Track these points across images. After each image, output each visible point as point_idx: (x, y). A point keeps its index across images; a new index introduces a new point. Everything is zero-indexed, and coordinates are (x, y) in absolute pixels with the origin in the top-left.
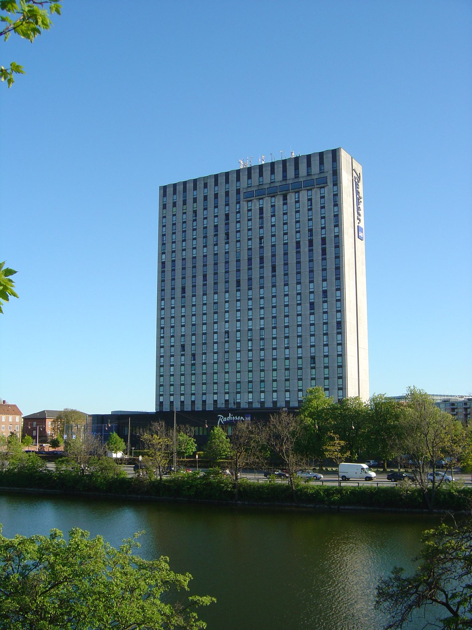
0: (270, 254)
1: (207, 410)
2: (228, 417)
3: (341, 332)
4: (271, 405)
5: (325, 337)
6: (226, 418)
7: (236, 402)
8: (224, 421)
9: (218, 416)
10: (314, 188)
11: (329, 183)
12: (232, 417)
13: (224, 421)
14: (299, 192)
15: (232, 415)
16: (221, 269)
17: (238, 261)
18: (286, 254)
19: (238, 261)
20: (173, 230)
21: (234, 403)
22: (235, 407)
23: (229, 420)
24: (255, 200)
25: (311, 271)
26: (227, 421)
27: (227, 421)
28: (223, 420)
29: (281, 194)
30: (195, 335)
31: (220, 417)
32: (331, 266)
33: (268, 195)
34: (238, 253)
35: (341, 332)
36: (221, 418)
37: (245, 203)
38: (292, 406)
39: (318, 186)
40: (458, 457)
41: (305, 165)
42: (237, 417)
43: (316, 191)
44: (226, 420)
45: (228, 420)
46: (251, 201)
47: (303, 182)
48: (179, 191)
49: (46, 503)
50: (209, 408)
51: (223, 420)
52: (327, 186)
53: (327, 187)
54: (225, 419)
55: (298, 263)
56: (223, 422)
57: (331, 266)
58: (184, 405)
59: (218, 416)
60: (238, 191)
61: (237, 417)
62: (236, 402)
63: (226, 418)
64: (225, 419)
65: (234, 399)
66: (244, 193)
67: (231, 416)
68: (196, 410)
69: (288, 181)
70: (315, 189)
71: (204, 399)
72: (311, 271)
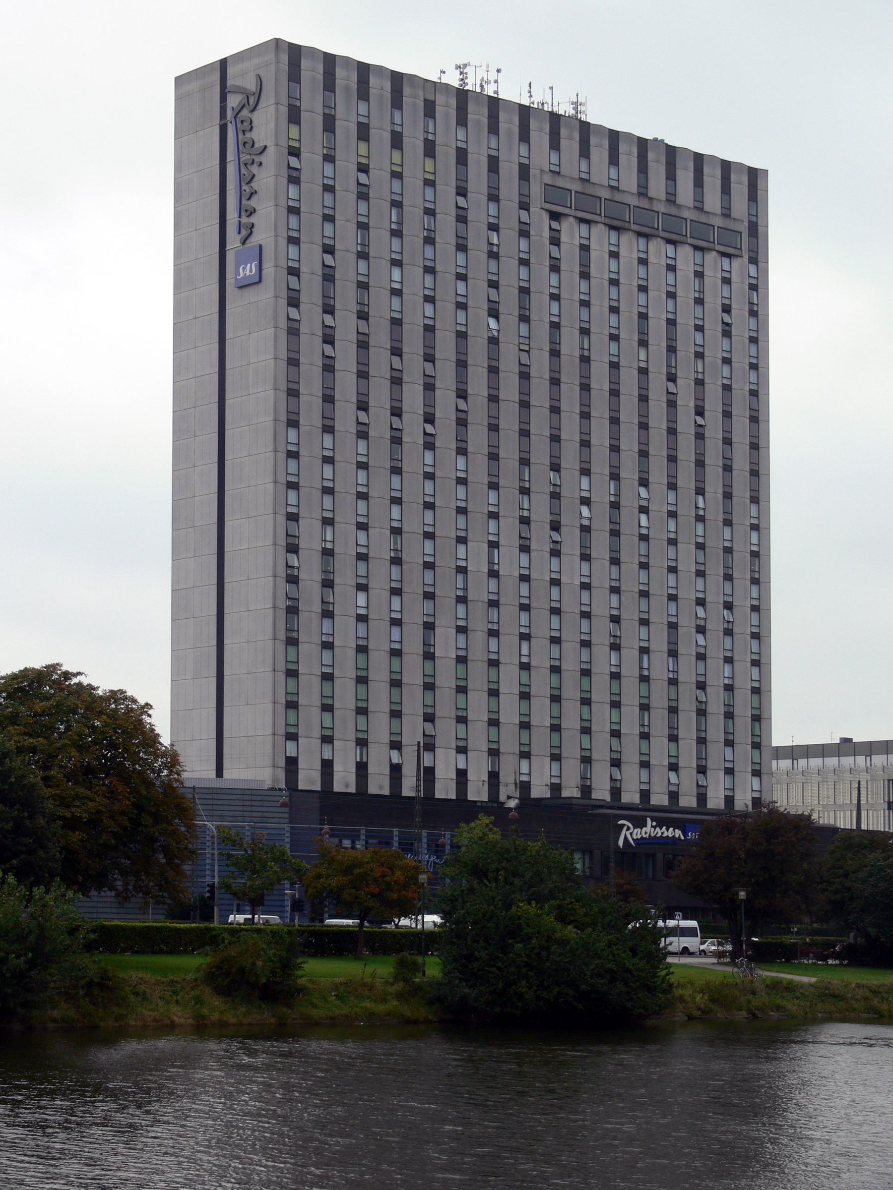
2: (644, 829)
4: (636, 799)
6: (639, 830)
7: (518, 782)
9: (620, 822)
10: (714, 250)
16: (600, 436)
21: (516, 783)
23: (647, 836)
26: (642, 837)
27: (642, 837)
28: (631, 834)
29: (546, 210)
31: (625, 825)
32: (741, 464)
42: (667, 830)
44: (639, 837)
45: (644, 836)
49: (813, 1156)
51: (631, 834)
52: (742, 257)
53: (740, 259)
54: (638, 833)
56: (632, 842)
57: (741, 464)
59: (620, 822)
61: (667, 830)
62: (518, 782)
67: (652, 826)
68: (403, 795)
70: (714, 253)
71: (327, 756)
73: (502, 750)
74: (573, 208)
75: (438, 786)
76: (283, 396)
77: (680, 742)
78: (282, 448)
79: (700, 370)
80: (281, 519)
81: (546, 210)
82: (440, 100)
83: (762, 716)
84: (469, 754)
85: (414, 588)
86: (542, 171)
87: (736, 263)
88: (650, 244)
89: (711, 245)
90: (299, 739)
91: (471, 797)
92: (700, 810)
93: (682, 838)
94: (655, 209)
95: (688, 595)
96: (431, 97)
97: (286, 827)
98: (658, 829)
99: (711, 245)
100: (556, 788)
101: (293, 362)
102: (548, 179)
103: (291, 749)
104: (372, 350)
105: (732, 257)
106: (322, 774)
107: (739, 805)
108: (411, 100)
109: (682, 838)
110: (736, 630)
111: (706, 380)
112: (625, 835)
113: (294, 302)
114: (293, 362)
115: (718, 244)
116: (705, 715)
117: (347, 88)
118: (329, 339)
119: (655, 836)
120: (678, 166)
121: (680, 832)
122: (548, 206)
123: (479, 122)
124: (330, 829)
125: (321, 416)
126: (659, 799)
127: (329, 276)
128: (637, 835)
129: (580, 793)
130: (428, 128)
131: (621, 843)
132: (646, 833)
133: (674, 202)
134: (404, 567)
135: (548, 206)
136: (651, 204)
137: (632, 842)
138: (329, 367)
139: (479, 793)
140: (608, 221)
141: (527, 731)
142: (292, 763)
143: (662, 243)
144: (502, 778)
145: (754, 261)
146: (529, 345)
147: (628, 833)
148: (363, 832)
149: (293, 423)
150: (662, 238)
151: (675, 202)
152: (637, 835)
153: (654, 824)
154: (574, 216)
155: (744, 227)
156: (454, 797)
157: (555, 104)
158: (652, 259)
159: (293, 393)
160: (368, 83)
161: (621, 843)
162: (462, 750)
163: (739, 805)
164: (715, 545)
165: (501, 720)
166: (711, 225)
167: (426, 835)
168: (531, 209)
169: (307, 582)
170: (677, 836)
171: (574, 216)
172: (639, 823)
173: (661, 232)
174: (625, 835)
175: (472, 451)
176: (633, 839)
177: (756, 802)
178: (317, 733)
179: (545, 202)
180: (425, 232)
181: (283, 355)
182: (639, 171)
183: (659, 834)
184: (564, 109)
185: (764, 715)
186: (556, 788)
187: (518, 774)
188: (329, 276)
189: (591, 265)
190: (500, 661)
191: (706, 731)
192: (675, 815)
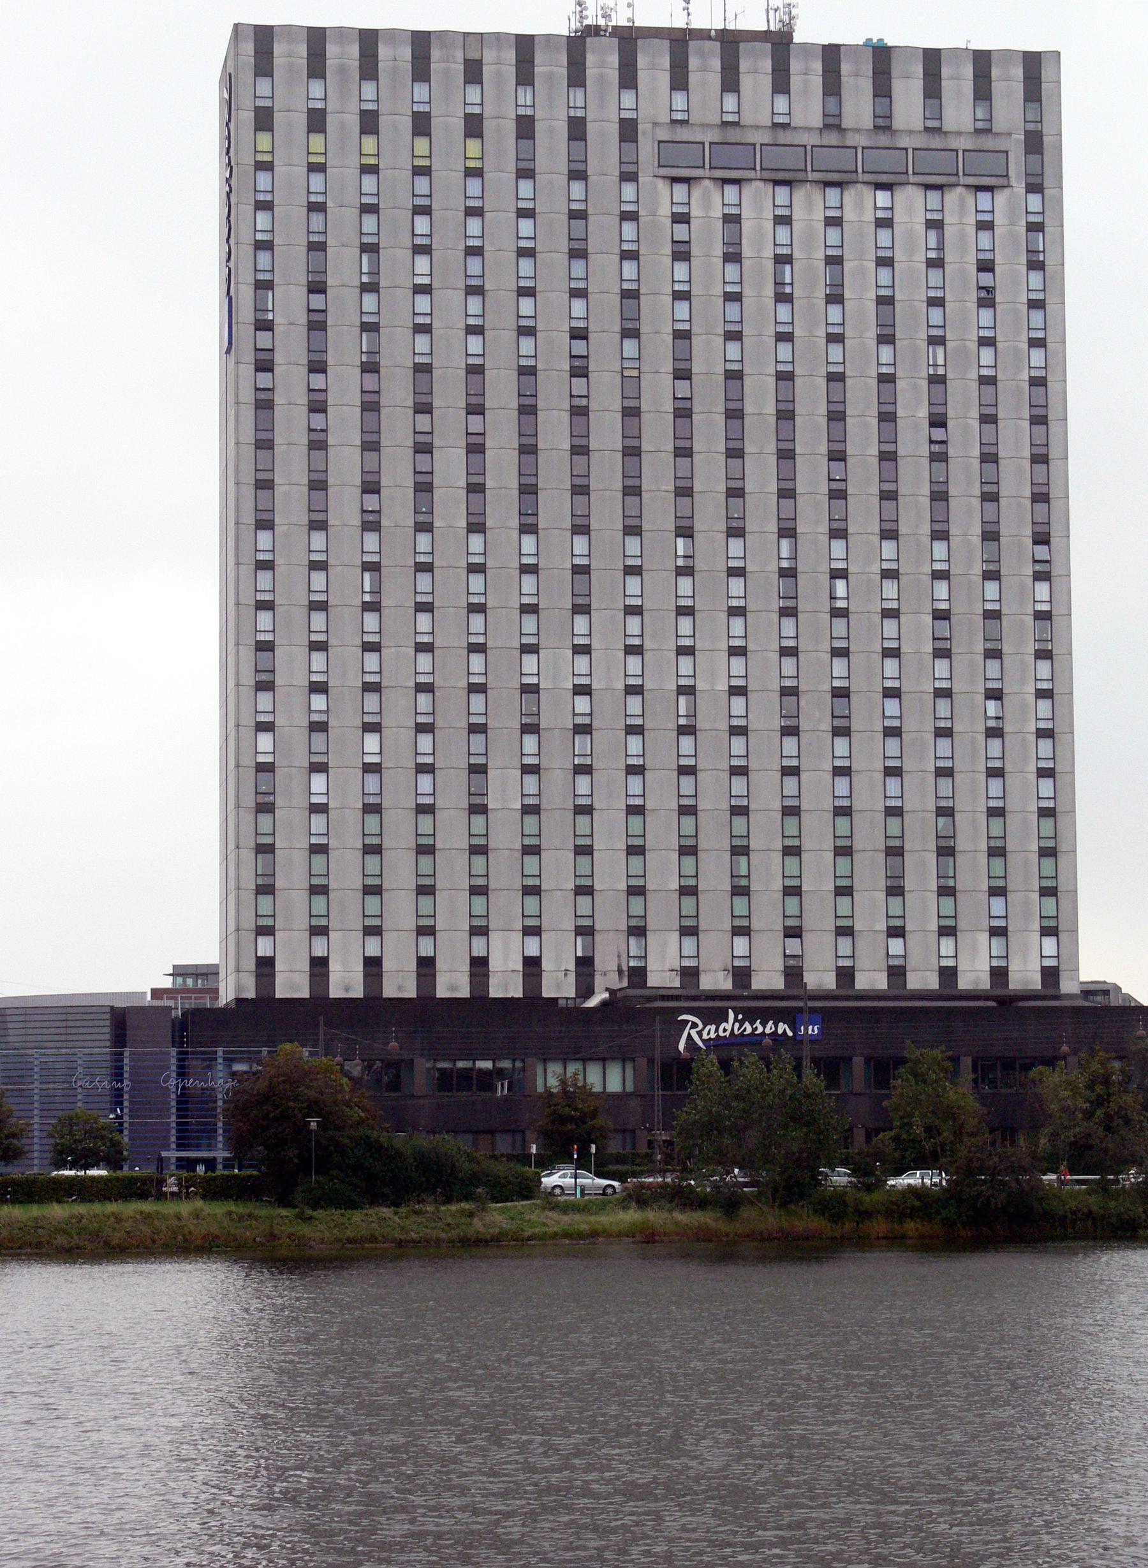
0: (771, 408)
1: (493, 994)
3: (1053, 730)
4: (777, 983)
6: (713, 1027)
7: (625, 968)
8: (705, 1037)
10: (958, 185)
11: (1013, 182)
12: (742, 1023)
13: (705, 1037)
15: (740, 1017)
17: (631, 413)
18: (837, 416)
19: (631, 413)
20: (518, 238)
22: (625, 983)
23: (728, 1033)
24: (707, 182)
25: (940, 496)
29: (664, 177)
31: (689, 1021)
33: (766, 175)
34: (631, 384)
35: (1053, 730)
36: (694, 1025)
37: (662, 187)
38: (918, 987)
40: (979, 1195)
41: (916, 85)
42: (764, 1025)
43: (962, 202)
44: (713, 1035)
45: (721, 1034)
47: (860, 150)
48: (395, 71)
51: (700, 1033)
52: (1009, 186)
53: (1007, 191)
54: (710, 1032)
55: (888, 457)
56: (700, 1044)
60: (628, 131)
61: (764, 1025)
62: (625, 968)
63: (713, 1027)
64: (710, 1032)
65: (619, 956)
66: (660, 142)
67: (736, 1020)
69: (849, 135)
70: (959, 190)
71: (319, 952)
72: (940, 496)
73: (597, 927)
74: (707, 166)
75: (493, 981)
76: (249, 491)
77: (907, 895)
78: (248, 559)
79: (941, 361)
80: (247, 653)
81: (664, 177)
82: (489, 56)
83: (1058, 849)
84: (544, 935)
85: (453, 720)
86: (655, 124)
87: (1001, 197)
88: (846, 194)
89: (952, 179)
90: (276, 933)
91: (547, 993)
92: (843, 992)
93: (790, 1034)
94: (849, 144)
95: (919, 686)
96: (473, 55)
97: (173, 1051)
98: (747, 1025)
99: (952, 179)
101: (264, 444)
102: (663, 135)
103: (264, 947)
104: (384, 411)
105: (995, 190)
106: (310, 976)
107: (1016, 982)
108: (596, 71)
109: (790, 1034)
110: (1007, 729)
111: (949, 376)
112: (689, 1034)
113: (264, 365)
114: (264, 444)
115: (964, 174)
116: (954, 855)
117: (499, 77)
118: (318, 406)
119: (742, 1035)
120: (894, 73)
121: (786, 1026)
122: (664, 172)
123: (447, 72)
124: (224, 1051)
125: (306, 509)
126: (716, 980)
127: (317, 324)
128: (709, 1034)
129: (678, 979)
131: (682, 1046)
132: (725, 1030)
133: (838, 128)
134: (437, 694)
135: (664, 172)
136: (844, 137)
137: (700, 1044)
138: (318, 444)
139: (558, 986)
140: (766, 175)
141: (899, 899)
142: (265, 966)
143: (867, 192)
144: (598, 964)
145: (1035, 187)
146: (639, 368)
147: (693, 1033)
148: (220, 1054)
149: (265, 524)
151: (940, 129)
152: (709, 1034)
154: (710, 178)
155: (1015, 145)
156: (519, 994)
157: (730, 15)
158: (849, 215)
159: (264, 485)
160: (375, 56)
161: (682, 1046)
162: (689, 931)
163: (1016, 982)
164: (968, 613)
165: (596, 887)
166: (802, 146)
167: (307, 1054)
169: (287, 729)
170: (780, 1031)
171: (710, 178)
172: (715, 1016)
173: (707, 171)
174: (689, 1034)
175: (545, 527)
176: (703, 1041)
177: (1051, 975)
178: (303, 923)
179: (659, 166)
181: (249, 436)
182: (927, 96)
183: (749, 1030)
185: (1063, 846)
186: (999, 974)
187: (624, 956)
188: (317, 324)
189: (743, 242)
190: (594, 806)
191: (954, 877)
192: (1032, 1003)
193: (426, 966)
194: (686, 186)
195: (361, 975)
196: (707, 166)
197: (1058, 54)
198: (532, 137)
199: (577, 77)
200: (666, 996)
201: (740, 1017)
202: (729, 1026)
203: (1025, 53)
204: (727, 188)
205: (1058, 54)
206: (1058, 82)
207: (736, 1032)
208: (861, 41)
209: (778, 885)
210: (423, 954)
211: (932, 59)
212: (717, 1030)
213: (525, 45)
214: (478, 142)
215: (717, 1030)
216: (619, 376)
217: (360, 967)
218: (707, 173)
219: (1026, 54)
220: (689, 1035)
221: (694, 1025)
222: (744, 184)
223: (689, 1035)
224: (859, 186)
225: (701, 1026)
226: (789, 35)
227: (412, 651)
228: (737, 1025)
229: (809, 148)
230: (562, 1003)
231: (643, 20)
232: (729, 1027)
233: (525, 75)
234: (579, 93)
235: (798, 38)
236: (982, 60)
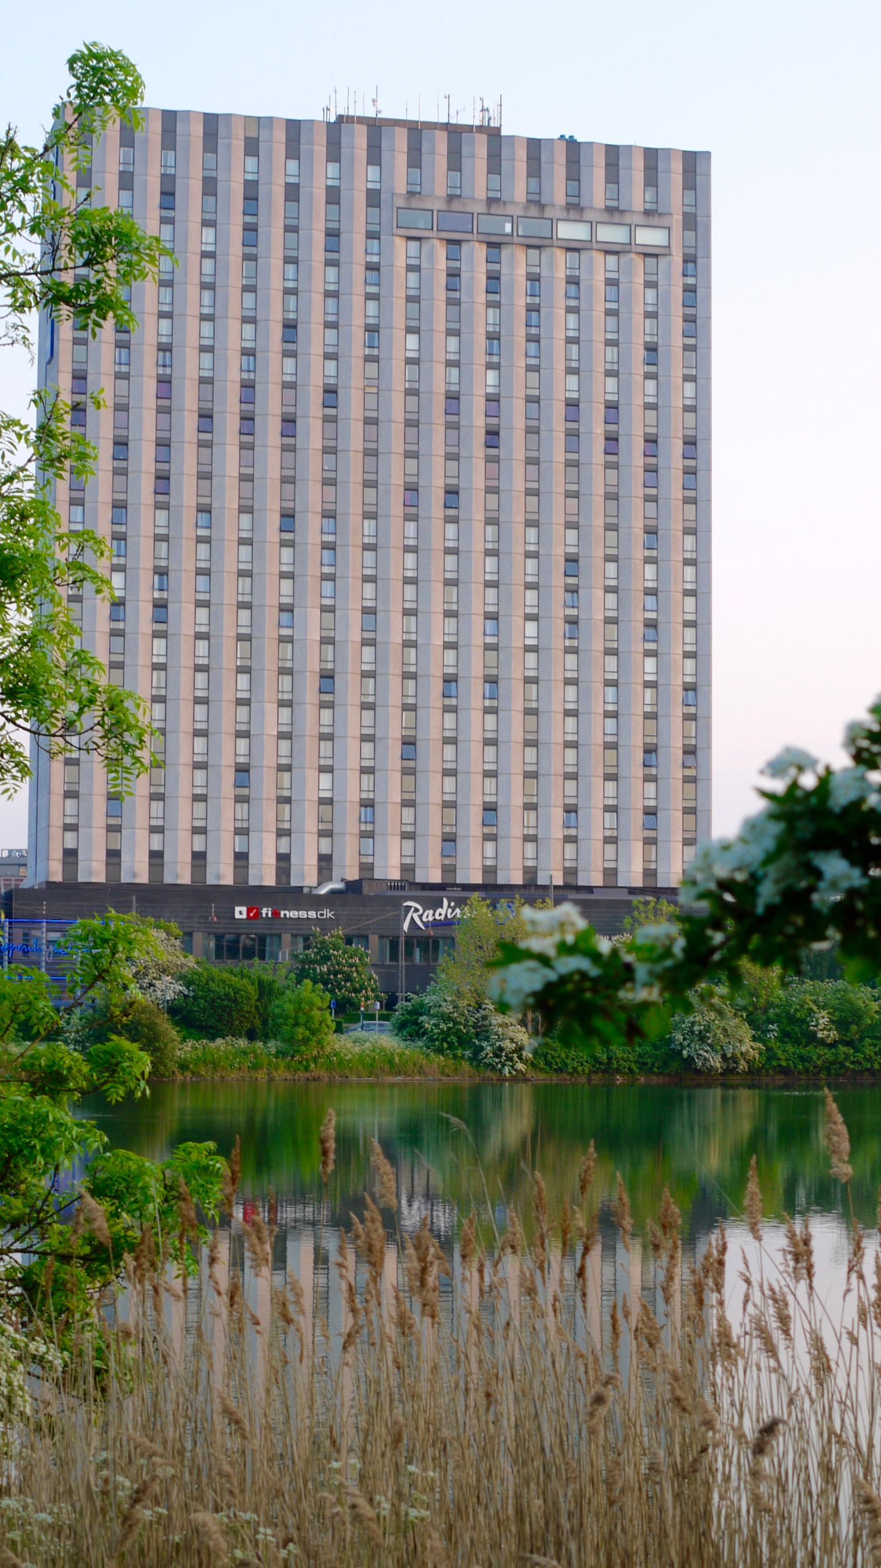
1: (80, 879)
2: (439, 910)
5: (648, 691)
6: (431, 912)
8: (424, 919)
9: (405, 904)
11: (674, 251)
13: (424, 919)
14: (499, 248)
23: (442, 918)
24: (435, 241)
28: (421, 917)
30: (656, 655)
36: (416, 910)
39: (401, 232)
41: (521, 167)
44: (431, 919)
45: (437, 917)
46: (418, 239)
50: (177, 876)
51: (421, 917)
53: (667, 259)
54: (429, 916)
58: (162, 865)
59: (405, 904)
63: (431, 912)
67: (449, 906)
71: (284, 850)
74: (435, 228)
98: (458, 911)
100: (611, 874)
130: (166, 161)
131: (406, 926)
132: (440, 915)
134: (212, 641)
147: (416, 917)
150: (558, 247)
153: (453, 904)
157: (453, 113)
161: (406, 926)
168: (382, 237)
180: (528, 298)
184: (469, 117)
185: (701, 775)
186: (611, 874)
193: (199, 858)
194: (418, 243)
195: (147, 865)
196: (435, 228)
197: (708, 154)
198: (297, 200)
199: (334, 153)
200: (394, 886)
201: (453, 904)
202: (443, 912)
203: (528, 139)
204: (531, 251)
205: (708, 154)
206: (709, 175)
207: (449, 916)
208: (556, 136)
209: (680, 805)
210: (196, 849)
211: (613, 152)
212: (434, 915)
213: (294, 127)
214: (128, 193)
215: (434, 915)
216: (362, 392)
217: (147, 859)
218: (434, 234)
219: (530, 141)
220: (412, 919)
221: (416, 910)
222: (423, 241)
223: (412, 919)
224: (555, 249)
225: (421, 911)
226: (499, 129)
227: (192, 606)
228: (450, 910)
229: (515, 218)
230: (306, 890)
231: (388, 113)
232: (443, 912)
233: (293, 150)
234: (171, 154)
235: (503, 133)
236: (651, 155)
